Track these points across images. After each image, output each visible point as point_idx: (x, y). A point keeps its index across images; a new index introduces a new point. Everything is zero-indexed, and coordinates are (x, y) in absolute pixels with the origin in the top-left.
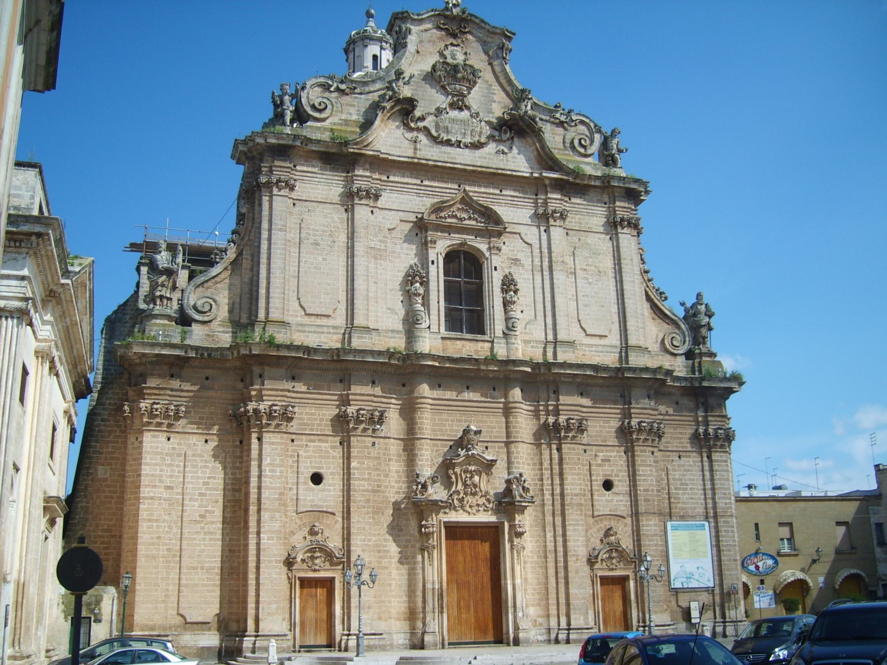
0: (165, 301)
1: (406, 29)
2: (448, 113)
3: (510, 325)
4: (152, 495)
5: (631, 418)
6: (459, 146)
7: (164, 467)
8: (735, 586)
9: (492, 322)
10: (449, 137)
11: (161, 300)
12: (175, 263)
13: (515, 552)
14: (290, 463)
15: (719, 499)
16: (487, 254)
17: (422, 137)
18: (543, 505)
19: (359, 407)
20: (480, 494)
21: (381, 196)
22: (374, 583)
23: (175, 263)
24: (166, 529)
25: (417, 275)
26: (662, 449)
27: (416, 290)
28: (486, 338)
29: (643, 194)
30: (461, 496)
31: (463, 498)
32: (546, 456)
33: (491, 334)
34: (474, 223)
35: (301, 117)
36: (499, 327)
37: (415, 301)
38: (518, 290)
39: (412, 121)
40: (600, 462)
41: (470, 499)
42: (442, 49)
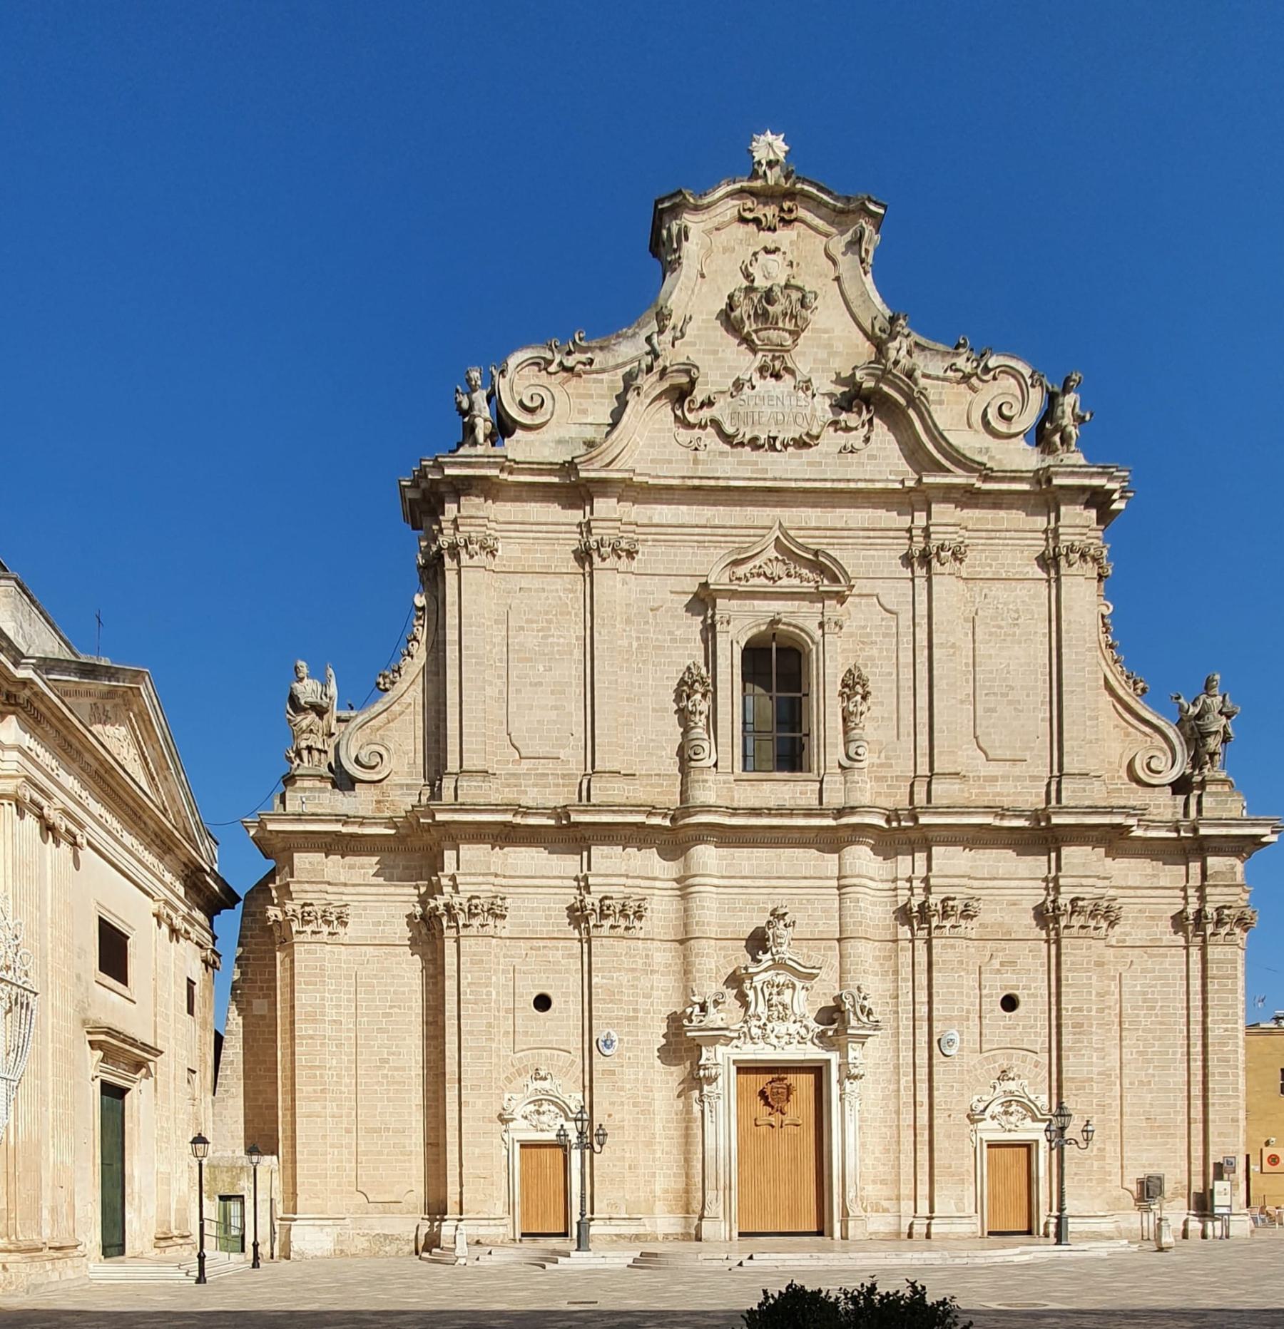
0: (315, 753)
1: (679, 230)
2: (753, 387)
3: (852, 754)
4: (311, 1032)
5: (1060, 894)
6: (773, 448)
7: (327, 995)
8: (1232, 1160)
9: (822, 749)
10: (756, 433)
11: (310, 753)
12: (326, 695)
13: (847, 1103)
14: (502, 981)
15: (1215, 1022)
16: (818, 634)
17: (709, 437)
18: (897, 1034)
19: (602, 895)
20: (793, 1018)
21: (637, 552)
22: (601, 1146)
23: (326, 695)
24: (335, 1079)
25: (697, 681)
26: (1114, 943)
27: (694, 705)
28: (813, 776)
29: (1116, 496)
30: (761, 1023)
31: (765, 1024)
32: (906, 958)
33: (819, 769)
34: (796, 581)
35: (503, 427)
36: (836, 754)
37: (692, 724)
38: (868, 693)
39: (690, 410)
40: (998, 967)
41: (780, 1028)
42: (747, 262)
